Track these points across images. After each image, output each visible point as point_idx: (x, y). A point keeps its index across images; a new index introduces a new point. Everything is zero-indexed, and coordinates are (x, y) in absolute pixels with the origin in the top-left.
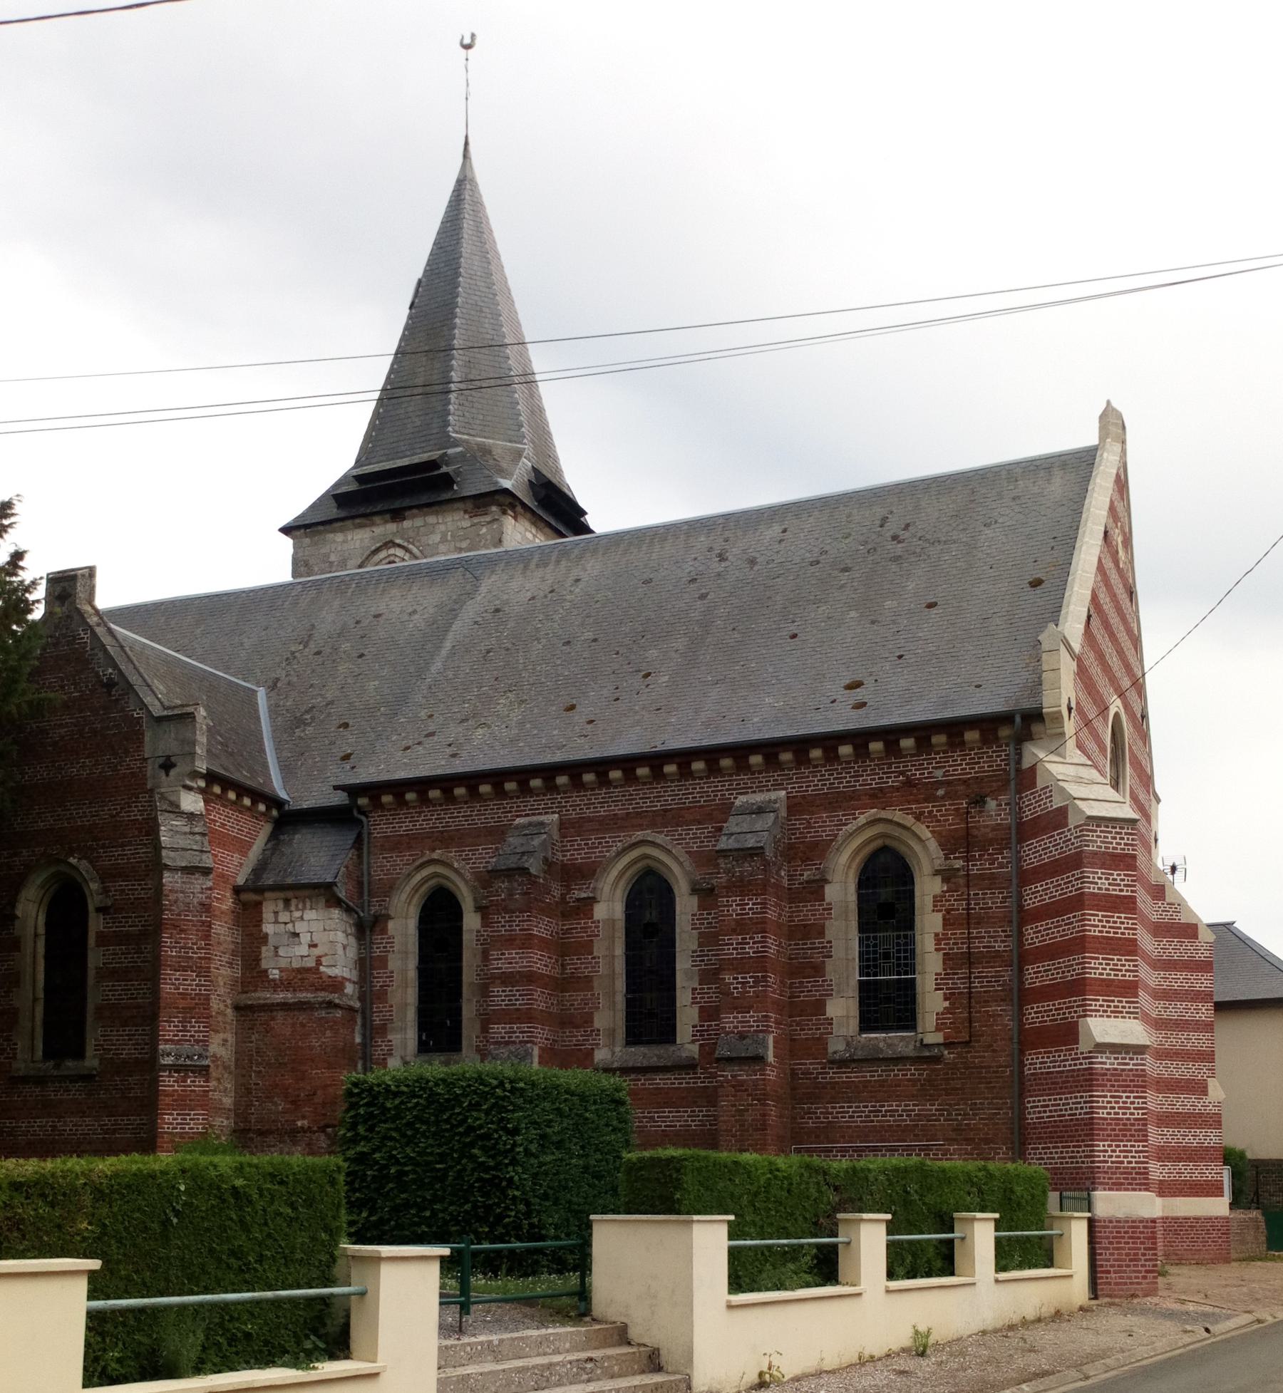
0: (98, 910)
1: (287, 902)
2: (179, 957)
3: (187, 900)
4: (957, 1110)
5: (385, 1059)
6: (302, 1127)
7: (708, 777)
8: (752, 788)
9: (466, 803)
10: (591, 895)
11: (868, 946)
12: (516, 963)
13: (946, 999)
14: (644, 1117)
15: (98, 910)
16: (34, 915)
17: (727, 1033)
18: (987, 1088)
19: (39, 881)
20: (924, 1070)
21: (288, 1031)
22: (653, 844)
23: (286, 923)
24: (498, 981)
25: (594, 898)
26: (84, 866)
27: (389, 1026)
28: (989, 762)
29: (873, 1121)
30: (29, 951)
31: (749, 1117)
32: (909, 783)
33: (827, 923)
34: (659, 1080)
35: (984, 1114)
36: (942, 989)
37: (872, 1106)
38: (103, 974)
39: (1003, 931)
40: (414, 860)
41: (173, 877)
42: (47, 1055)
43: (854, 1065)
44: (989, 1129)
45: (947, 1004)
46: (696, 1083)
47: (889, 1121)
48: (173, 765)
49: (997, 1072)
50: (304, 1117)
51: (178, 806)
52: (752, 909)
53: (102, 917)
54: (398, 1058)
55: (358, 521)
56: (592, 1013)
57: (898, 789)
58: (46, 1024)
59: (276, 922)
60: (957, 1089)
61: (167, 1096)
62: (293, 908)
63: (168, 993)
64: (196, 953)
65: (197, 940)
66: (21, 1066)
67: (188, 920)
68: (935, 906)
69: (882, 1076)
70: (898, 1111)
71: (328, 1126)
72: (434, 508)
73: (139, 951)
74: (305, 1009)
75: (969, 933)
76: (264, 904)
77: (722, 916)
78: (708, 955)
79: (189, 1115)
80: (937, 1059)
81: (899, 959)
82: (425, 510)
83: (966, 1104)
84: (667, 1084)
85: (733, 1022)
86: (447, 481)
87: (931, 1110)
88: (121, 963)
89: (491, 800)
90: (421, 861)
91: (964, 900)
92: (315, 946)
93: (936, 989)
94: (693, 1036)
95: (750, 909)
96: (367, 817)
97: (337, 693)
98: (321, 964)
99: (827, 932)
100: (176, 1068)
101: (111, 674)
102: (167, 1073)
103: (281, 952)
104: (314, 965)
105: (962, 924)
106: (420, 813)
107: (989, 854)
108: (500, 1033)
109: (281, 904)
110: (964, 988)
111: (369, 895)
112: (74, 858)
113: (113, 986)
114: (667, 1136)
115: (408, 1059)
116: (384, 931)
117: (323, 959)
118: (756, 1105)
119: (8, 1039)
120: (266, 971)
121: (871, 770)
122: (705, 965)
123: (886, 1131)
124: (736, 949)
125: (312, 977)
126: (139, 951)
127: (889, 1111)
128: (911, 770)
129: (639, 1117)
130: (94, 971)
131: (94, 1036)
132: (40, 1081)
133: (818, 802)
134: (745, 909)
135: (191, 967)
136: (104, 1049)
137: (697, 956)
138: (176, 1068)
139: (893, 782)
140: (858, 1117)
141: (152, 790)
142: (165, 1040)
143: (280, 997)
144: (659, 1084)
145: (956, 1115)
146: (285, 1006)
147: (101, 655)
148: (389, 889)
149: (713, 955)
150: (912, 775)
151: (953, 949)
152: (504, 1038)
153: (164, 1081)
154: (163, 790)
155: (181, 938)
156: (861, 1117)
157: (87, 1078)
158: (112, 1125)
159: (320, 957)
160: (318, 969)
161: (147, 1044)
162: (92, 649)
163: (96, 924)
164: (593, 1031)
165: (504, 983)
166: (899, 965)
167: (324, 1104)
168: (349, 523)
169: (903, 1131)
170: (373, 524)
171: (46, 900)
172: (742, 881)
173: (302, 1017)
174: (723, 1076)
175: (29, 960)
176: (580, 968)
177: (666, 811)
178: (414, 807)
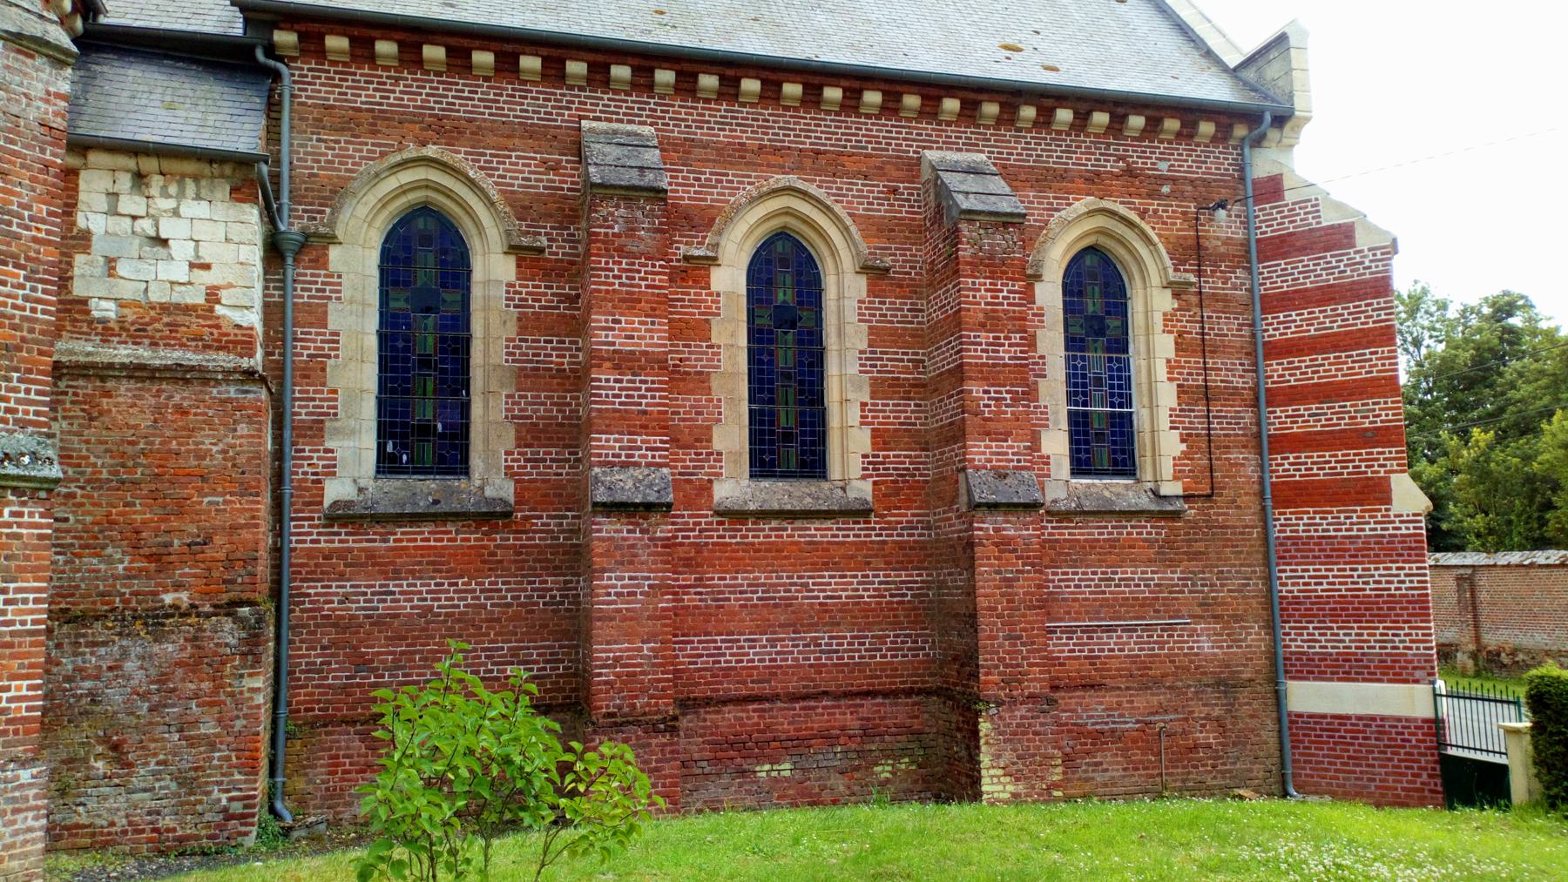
1: (140, 178)
4: (1203, 579)
6: (175, 607)
7: (878, 117)
8: (938, 142)
9: (487, 79)
10: (710, 254)
11: (1075, 367)
12: (640, 338)
13: (1183, 441)
14: (792, 584)
17: (977, 469)
18: (1233, 553)
20: (1162, 528)
21: (145, 421)
22: (804, 195)
23: (134, 218)
24: (608, 364)
25: (715, 259)
27: (327, 424)
28: (1213, 164)
29: (1104, 593)
31: (1020, 589)
32: (1130, 172)
33: (1039, 332)
34: (816, 531)
35: (1234, 584)
36: (1177, 428)
37: (1102, 573)
39: (1241, 364)
40: (383, 154)
43: (1078, 519)
44: (1238, 604)
45: (1183, 447)
46: (870, 536)
47: (1124, 592)
49: (1243, 533)
50: (178, 587)
52: (1008, 298)
54: (349, 482)
56: (709, 428)
57: (1117, 177)
59: (113, 212)
60: (1201, 553)
62: (154, 190)
64: (27, 228)
68: (1166, 326)
69: (1112, 533)
70: (1137, 578)
71: (242, 603)
75: (1205, 363)
76: (83, 175)
77: (966, 303)
78: (882, 359)
80: (1175, 515)
81: (1112, 386)
83: (1211, 572)
84: (826, 536)
85: (984, 453)
87: (1172, 579)
89: (534, 83)
90: (398, 158)
91: (1197, 322)
93: (1171, 428)
94: (864, 469)
95: (1004, 298)
98: (218, 302)
99: (1038, 344)
103: (123, 269)
105: (1194, 351)
106: (397, 79)
107: (1221, 272)
108: (613, 448)
109: (125, 181)
110: (1202, 429)
114: (826, 611)
115: (363, 483)
116: (321, 262)
117: (224, 295)
118: (1029, 572)
120: (84, 302)
121: (1086, 147)
122: (878, 372)
123: (1121, 606)
124: (986, 351)
125: (195, 323)
127: (1124, 579)
128: (1132, 157)
129: (784, 585)
133: (1023, 177)
134: (997, 297)
135: (15, 256)
137: (867, 359)
139: (1112, 167)
140: (1086, 586)
143: (123, 353)
144: (815, 536)
145: (1202, 585)
146: (138, 372)
148: (333, 194)
149: (888, 360)
150: (1133, 162)
151: (1187, 380)
152: (619, 456)
156: (1090, 586)
159: (218, 288)
160: (211, 310)
164: (712, 454)
165: (617, 368)
166: (1112, 395)
167: (230, 562)
169: (1142, 606)
172: (991, 257)
174: (981, 529)
176: (688, 359)
177: (818, 153)
178: (386, 68)
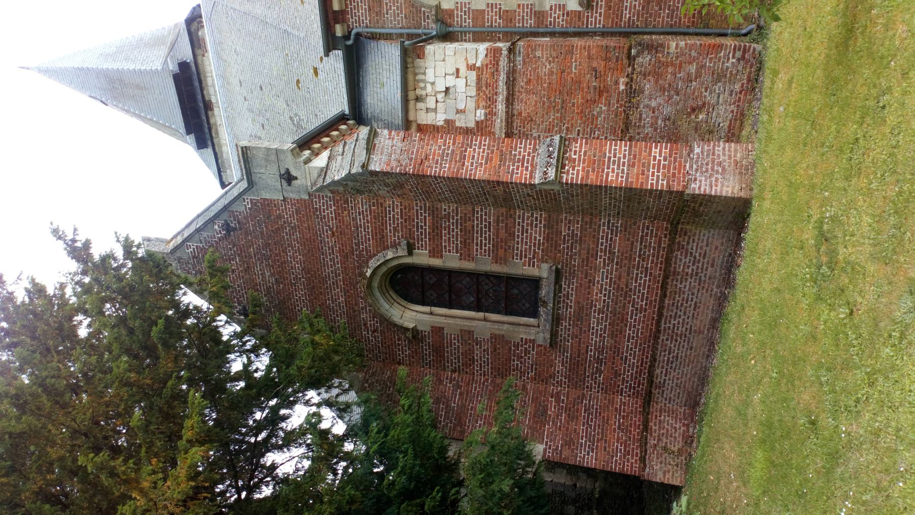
0: (410, 253)
1: (418, 99)
2: (451, 161)
3: (399, 151)
5: (568, 13)
15: (410, 253)
16: (415, 314)
19: (387, 306)
23: (437, 101)
26: (373, 263)
27: (537, 9)
30: (442, 320)
38: (466, 252)
41: (376, 162)
42: (535, 314)
48: (288, 172)
51: (322, 169)
53: (416, 251)
55: (214, 135)
58: (508, 312)
59: (435, 110)
61: (588, 176)
62: (424, 93)
63: (484, 173)
64: (449, 147)
65: (437, 145)
66: (542, 336)
67: (417, 152)
72: (203, 78)
73: (448, 217)
74: (514, 79)
76: (419, 122)
79: (610, 158)
82: (204, 85)
86: (183, 66)
88: (457, 234)
92: (458, 70)
96: (352, 29)
97: (281, 100)
98: (474, 65)
100: (561, 167)
101: (219, 227)
102: (565, 176)
104: (474, 73)
109: (420, 105)
111: (419, 28)
112: (367, 271)
113: (477, 245)
116: (450, 13)
119: (517, 346)
120: (477, 123)
125: (486, 76)
126: (448, 217)
130: (463, 261)
131: (521, 268)
132: (556, 320)
135: (462, 152)
136: (534, 258)
138: (561, 167)
141: (310, 195)
142: (531, 177)
143: (501, 107)
146: (510, 100)
147: (205, 234)
153: (572, 178)
154: (309, 184)
155: (433, 159)
157: (558, 274)
158: (605, 255)
159: (468, 65)
160: (479, 68)
161: (532, 215)
162: (201, 243)
163: (422, 258)
168: (215, 141)
170: (215, 124)
171: (404, 303)
173: (521, 82)
175: (451, 321)
